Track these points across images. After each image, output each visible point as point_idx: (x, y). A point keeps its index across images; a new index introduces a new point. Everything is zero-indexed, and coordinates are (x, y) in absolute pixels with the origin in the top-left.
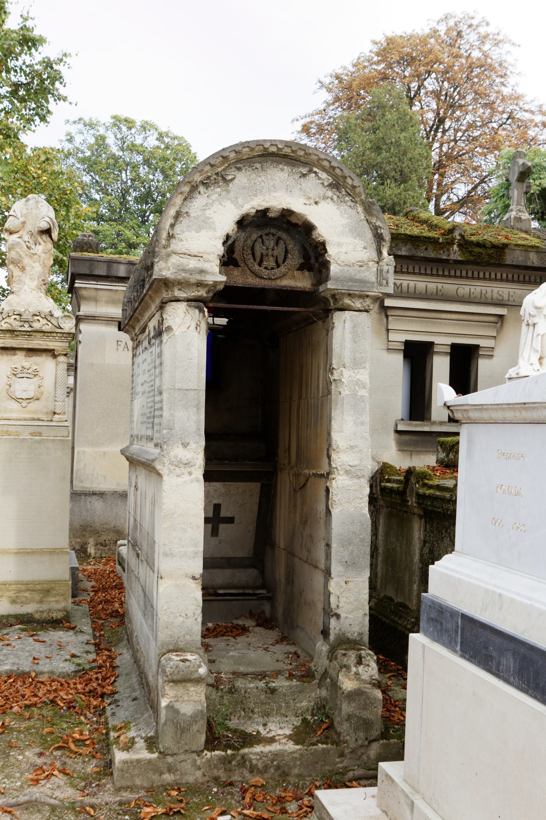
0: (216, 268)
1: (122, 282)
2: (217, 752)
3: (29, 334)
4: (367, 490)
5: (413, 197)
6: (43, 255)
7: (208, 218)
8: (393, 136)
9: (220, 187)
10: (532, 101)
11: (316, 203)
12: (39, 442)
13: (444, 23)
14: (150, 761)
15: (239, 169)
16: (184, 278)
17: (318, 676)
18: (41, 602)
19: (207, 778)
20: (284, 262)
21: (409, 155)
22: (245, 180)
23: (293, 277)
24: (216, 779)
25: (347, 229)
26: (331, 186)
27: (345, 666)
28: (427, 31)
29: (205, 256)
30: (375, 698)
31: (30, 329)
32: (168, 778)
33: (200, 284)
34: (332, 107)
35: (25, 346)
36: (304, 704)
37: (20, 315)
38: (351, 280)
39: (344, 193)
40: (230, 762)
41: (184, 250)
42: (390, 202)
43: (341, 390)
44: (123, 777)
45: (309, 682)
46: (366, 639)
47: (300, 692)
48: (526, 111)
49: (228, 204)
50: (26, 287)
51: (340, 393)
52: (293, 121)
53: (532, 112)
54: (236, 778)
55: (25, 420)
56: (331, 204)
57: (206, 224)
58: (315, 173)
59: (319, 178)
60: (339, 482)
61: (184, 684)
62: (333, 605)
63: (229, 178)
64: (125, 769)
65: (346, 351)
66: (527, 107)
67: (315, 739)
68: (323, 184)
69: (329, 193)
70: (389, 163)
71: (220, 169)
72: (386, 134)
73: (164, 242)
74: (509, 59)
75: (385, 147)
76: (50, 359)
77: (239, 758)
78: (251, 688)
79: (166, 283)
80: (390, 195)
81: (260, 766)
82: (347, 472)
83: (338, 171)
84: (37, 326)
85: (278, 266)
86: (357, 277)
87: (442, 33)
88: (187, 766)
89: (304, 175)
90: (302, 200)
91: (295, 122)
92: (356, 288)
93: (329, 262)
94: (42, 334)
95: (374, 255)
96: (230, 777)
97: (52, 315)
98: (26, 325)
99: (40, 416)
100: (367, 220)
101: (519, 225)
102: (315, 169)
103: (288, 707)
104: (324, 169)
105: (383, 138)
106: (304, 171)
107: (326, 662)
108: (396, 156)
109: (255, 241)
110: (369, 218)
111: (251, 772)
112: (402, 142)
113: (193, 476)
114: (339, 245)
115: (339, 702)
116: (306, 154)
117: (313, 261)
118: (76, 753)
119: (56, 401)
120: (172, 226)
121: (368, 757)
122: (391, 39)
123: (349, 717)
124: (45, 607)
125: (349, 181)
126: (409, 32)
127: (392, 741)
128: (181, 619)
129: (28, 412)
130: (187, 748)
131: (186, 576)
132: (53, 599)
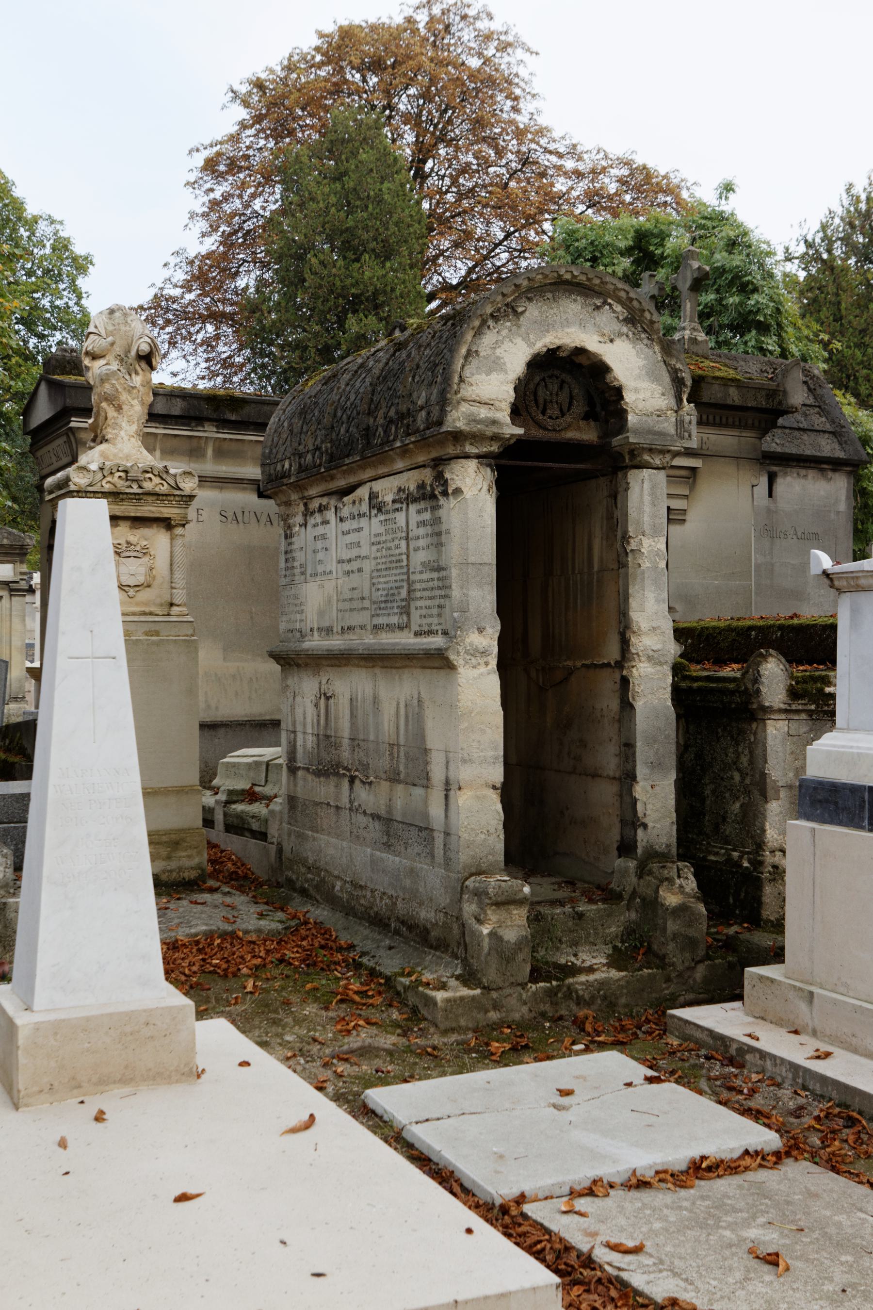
0: (504, 416)
1: (184, 425)
2: (542, 984)
3: (138, 497)
4: (670, 680)
5: (404, 282)
6: (141, 389)
7: (498, 358)
8: (372, 187)
9: (510, 320)
10: (563, 138)
11: (612, 341)
12: (158, 644)
13: (426, 11)
14: (473, 998)
15: (530, 299)
16: (479, 431)
17: (626, 896)
18: (169, 858)
19: (533, 1014)
20: (569, 410)
21: (395, 217)
22: (536, 313)
23: (579, 429)
24: (543, 1014)
25: (644, 372)
26: (626, 321)
27: (667, 879)
28: (399, 20)
29: (497, 403)
30: (699, 914)
31: (140, 491)
32: (494, 1016)
33: (495, 438)
34: (249, 132)
35: (133, 514)
36: (613, 929)
37: (126, 472)
38: (650, 432)
39: (640, 329)
40: (556, 994)
41: (474, 397)
42: (371, 289)
43: (640, 561)
44: (447, 1018)
45: (617, 904)
46: (674, 851)
47: (609, 916)
48: (551, 152)
49: (519, 341)
50: (122, 433)
51: (640, 565)
52: (190, 152)
53: (560, 156)
54: (563, 1012)
55: (134, 614)
56: (627, 342)
57: (496, 365)
58: (610, 305)
59: (614, 312)
60: (641, 670)
61: (506, 907)
62: (640, 814)
63: (520, 310)
64: (449, 1008)
65: (646, 515)
66: (552, 147)
67: (637, 965)
68: (618, 318)
69: (625, 330)
70: (366, 228)
71: (509, 300)
72: (360, 183)
73: (455, 387)
74: (523, 72)
75: (358, 203)
76: (163, 531)
77: (565, 989)
78: (558, 914)
79: (458, 436)
80: (370, 278)
81: (587, 997)
82: (649, 658)
83: (635, 303)
84: (148, 486)
85: (563, 414)
86: (656, 428)
87: (421, 26)
88: (513, 1001)
89: (598, 308)
90: (596, 338)
91: (195, 154)
92: (658, 442)
93: (626, 411)
94: (154, 498)
95: (673, 403)
96: (557, 1011)
97: (167, 472)
98: (135, 486)
99: (153, 609)
100: (665, 362)
101: (695, 348)
102: (609, 301)
103: (596, 934)
104: (619, 301)
105: (355, 189)
106: (598, 302)
107: (634, 880)
108: (376, 219)
109: (538, 384)
110: (668, 359)
111: (578, 1004)
112: (386, 197)
113: (490, 667)
114: (636, 390)
115: (660, 922)
116: (602, 282)
117: (598, 409)
118: (364, 1004)
119: (172, 588)
120: (463, 366)
121: (694, 980)
122: (347, 32)
123: (675, 936)
124: (173, 865)
125: (647, 315)
126: (372, 20)
127: (717, 961)
128: (483, 836)
129: (137, 604)
130: (512, 980)
131: (487, 785)
132: (184, 854)
